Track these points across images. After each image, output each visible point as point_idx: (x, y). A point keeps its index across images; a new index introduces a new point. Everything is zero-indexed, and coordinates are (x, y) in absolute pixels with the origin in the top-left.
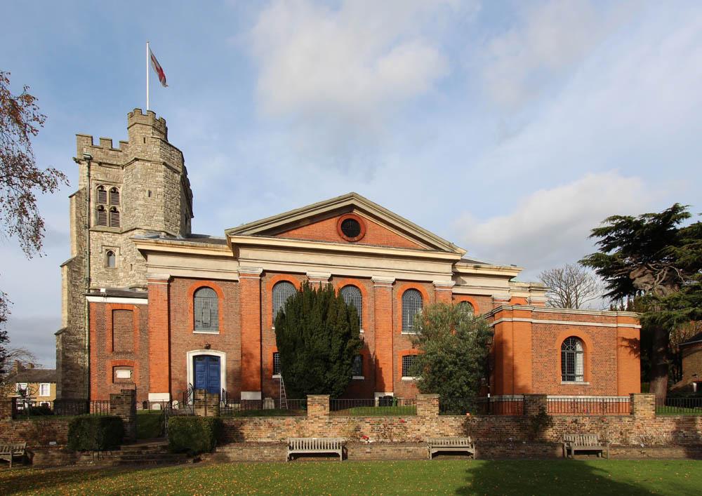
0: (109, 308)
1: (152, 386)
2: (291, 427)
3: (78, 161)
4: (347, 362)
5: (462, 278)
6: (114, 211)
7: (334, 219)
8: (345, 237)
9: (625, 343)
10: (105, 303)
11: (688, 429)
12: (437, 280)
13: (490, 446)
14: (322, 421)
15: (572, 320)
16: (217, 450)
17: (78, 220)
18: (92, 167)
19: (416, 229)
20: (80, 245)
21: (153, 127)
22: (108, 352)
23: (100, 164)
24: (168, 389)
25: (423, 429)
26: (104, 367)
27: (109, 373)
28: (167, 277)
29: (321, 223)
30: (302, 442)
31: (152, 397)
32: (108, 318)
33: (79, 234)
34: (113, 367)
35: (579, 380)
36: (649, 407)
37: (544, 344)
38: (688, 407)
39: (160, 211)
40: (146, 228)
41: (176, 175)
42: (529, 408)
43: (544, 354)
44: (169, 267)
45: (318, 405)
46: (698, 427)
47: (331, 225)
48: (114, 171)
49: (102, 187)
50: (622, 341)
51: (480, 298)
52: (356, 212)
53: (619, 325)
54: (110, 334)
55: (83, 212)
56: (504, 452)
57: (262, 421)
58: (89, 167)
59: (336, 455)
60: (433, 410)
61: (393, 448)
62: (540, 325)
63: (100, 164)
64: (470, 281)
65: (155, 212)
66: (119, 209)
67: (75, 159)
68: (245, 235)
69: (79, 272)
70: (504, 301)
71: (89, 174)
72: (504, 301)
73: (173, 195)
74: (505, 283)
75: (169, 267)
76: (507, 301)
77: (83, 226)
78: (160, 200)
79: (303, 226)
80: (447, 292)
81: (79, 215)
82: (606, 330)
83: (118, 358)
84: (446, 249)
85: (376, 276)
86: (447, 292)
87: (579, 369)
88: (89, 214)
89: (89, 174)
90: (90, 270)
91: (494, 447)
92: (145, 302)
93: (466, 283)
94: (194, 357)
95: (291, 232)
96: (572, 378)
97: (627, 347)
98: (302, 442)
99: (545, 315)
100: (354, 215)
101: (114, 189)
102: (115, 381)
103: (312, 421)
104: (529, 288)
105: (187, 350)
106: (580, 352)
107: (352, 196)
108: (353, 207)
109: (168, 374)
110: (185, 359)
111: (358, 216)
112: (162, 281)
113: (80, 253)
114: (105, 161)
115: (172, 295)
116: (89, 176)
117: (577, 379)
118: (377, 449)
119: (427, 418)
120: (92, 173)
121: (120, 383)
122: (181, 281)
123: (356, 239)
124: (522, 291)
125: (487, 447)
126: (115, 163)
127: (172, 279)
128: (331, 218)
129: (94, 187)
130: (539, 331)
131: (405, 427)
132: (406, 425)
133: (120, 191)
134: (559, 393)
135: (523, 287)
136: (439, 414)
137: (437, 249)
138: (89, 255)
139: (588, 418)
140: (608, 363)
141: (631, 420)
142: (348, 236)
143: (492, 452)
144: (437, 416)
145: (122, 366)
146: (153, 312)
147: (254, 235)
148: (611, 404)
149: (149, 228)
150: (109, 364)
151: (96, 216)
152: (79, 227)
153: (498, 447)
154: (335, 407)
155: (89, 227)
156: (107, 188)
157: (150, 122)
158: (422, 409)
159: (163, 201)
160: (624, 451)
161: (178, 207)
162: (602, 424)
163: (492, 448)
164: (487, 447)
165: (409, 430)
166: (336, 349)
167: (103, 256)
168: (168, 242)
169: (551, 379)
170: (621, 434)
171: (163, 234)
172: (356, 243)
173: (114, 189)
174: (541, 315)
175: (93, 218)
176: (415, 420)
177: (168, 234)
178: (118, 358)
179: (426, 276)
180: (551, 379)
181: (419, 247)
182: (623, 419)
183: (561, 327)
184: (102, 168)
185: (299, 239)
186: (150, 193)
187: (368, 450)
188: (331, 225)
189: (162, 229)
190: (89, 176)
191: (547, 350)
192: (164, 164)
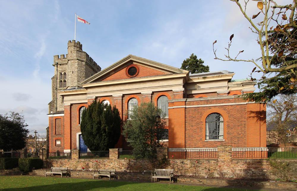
0: (54, 118)
1: (65, 147)
2: (67, 163)
3: (54, 66)
4: (104, 134)
5: (198, 85)
6: (65, 81)
7: (125, 69)
8: (129, 76)
9: (253, 115)
10: (53, 117)
11: (255, 168)
12: (174, 89)
13: (124, 174)
14: (76, 161)
15: (213, 103)
16: (33, 171)
17: (53, 87)
18: (58, 67)
19: (161, 65)
20: (54, 96)
21: (74, 46)
22: (54, 135)
23: (60, 65)
24: (70, 148)
25: (112, 165)
26: (53, 140)
27: (54, 142)
28: (69, 104)
29: (119, 71)
30: (166, 171)
31: (65, 151)
32: (54, 122)
33: (53, 92)
34: (56, 140)
35: (221, 138)
36: (228, 154)
37: (194, 119)
38: (127, 154)
39: (76, 78)
40: (71, 86)
41: (83, 62)
42: (159, 155)
43: (194, 124)
44: (70, 100)
45: (113, 153)
46: (264, 167)
47: (124, 71)
48: (65, 66)
49: (61, 73)
50: (250, 114)
51: (210, 94)
52: (134, 63)
53: (187, 107)
54: (55, 128)
55: (55, 84)
56: (130, 177)
57: (58, 160)
58: (57, 67)
59: (60, 175)
60: (116, 156)
61: (87, 173)
62: (192, 109)
63: (60, 65)
64: (202, 86)
65: (74, 79)
66: (66, 80)
67: (53, 65)
68: (88, 83)
69: (53, 106)
70: (224, 94)
71: (57, 69)
72: (224, 94)
73: (81, 71)
74: (226, 83)
75: (70, 100)
76: (226, 94)
77: (55, 89)
78: (76, 74)
79: (112, 75)
80: (180, 95)
81: (54, 85)
82: (239, 107)
83: (57, 137)
84: (179, 72)
85: (143, 92)
86: (180, 95)
87: (221, 132)
88: (57, 84)
89: (57, 69)
90: (57, 105)
91: (126, 175)
92: (63, 115)
93: (200, 87)
94: (79, 135)
95: (107, 79)
96: (217, 137)
97: (254, 117)
98: (166, 171)
99: (195, 102)
100: (134, 65)
101: (65, 73)
102: (56, 145)
103: (73, 161)
104: (242, 84)
105: (77, 132)
106: (222, 122)
107: (129, 57)
108: (131, 61)
109: (70, 142)
110: (76, 136)
111: (136, 65)
112: (69, 106)
113: (53, 99)
114: (62, 63)
115: (72, 111)
116: (57, 70)
117: (220, 138)
118: (81, 173)
119: (113, 160)
120: (58, 69)
121: (57, 146)
122: (75, 105)
123: (134, 76)
124: (238, 86)
125: (123, 175)
126: (65, 63)
127: (72, 105)
128: (124, 68)
129: (59, 74)
130: (191, 112)
131: (105, 164)
132: (105, 163)
133: (66, 73)
134: (204, 146)
135: (238, 84)
136: (118, 158)
137: (174, 73)
138: (57, 99)
139: (189, 161)
140: (240, 127)
141: (215, 162)
142: (132, 75)
143: (125, 177)
144: (117, 159)
145: (58, 140)
146: (65, 119)
147: (90, 83)
148: (242, 153)
149: (72, 86)
150: (54, 139)
151: (59, 84)
152: (53, 89)
153: (127, 175)
154: (120, 154)
155: (57, 89)
156: (63, 73)
157: (73, 44)
158: (111, 156)
159: (77, 74)
160: (189, 180)
161: (84, 75)
162: (198, 164)
163: (125, 175)
164: (123, 175)
165: (106, 165)
166: (94, 129)
167: (61, 99)
168: (80, 90)
169: (199, 138)
170: (209, 170)
171: (77, 87)
172: (136, 77)
173: (65, 73)
174: (203, 102)
175: (58, 85)
176: (108, 161)
177: (79, 87)
178: (57, 137)
179: (168, 88)
180: (199, 138)
181: (166, 74)
182: (210, 161)
183: (205, 108)
184: (61, 66)
185: (113, 80)
186: (73, 72)
187: (78, 174)
188: (124, 71)
189: (76, 85)
190: (57, 70)
191: (196, 122)
192: (77, 59)
